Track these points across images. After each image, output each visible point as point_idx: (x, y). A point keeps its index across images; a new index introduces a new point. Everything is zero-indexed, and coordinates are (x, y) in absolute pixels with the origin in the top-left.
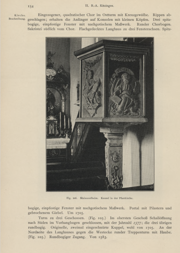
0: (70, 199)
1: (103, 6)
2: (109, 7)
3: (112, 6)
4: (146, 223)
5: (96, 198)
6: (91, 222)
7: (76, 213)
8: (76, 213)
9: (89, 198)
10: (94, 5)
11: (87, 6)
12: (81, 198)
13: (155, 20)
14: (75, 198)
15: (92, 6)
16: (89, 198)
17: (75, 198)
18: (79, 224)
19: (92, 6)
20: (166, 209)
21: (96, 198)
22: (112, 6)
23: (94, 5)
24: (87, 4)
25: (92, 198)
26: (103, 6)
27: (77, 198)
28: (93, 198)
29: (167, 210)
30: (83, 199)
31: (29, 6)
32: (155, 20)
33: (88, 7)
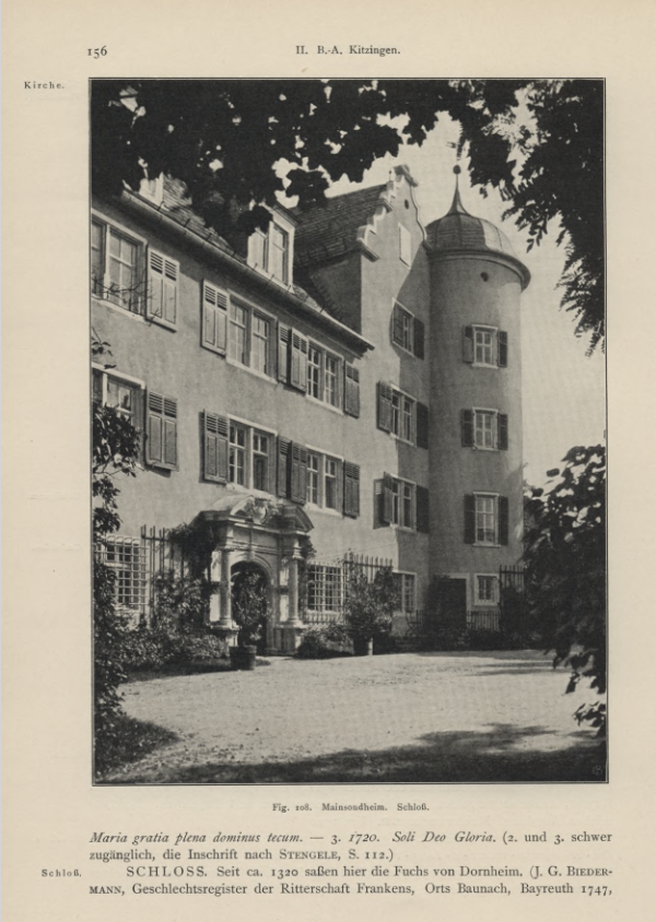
0: (284, 811)
1: (362, 50)
2: (382, 54)
3: (394, 51)
4: (168, 855)
5: (381, 808)
6: (166, 885)
7: (584, 887)
8: (584, 887)
9: (355, 808)
10: (328, 47)
11: (300, 49)
12: (326, 807)
13: (465, 870)
14: (306, 807)
15: (320, 49)
16: (355, 808)
17: (306, 807)
18: (335, 877)
19: (320, 49)
20: (528, 838)
21: (381, 808)
22: (394, 51)
23: (328, 47)
24: (300, 45)
25: (363, 807)
26: (362, 50)
27: (321, 806)
28: (367, 808)
29: (531, 842)
30: (333, 809)
31: (92, 51)
32: (465, 870)
33: (304, 55)
